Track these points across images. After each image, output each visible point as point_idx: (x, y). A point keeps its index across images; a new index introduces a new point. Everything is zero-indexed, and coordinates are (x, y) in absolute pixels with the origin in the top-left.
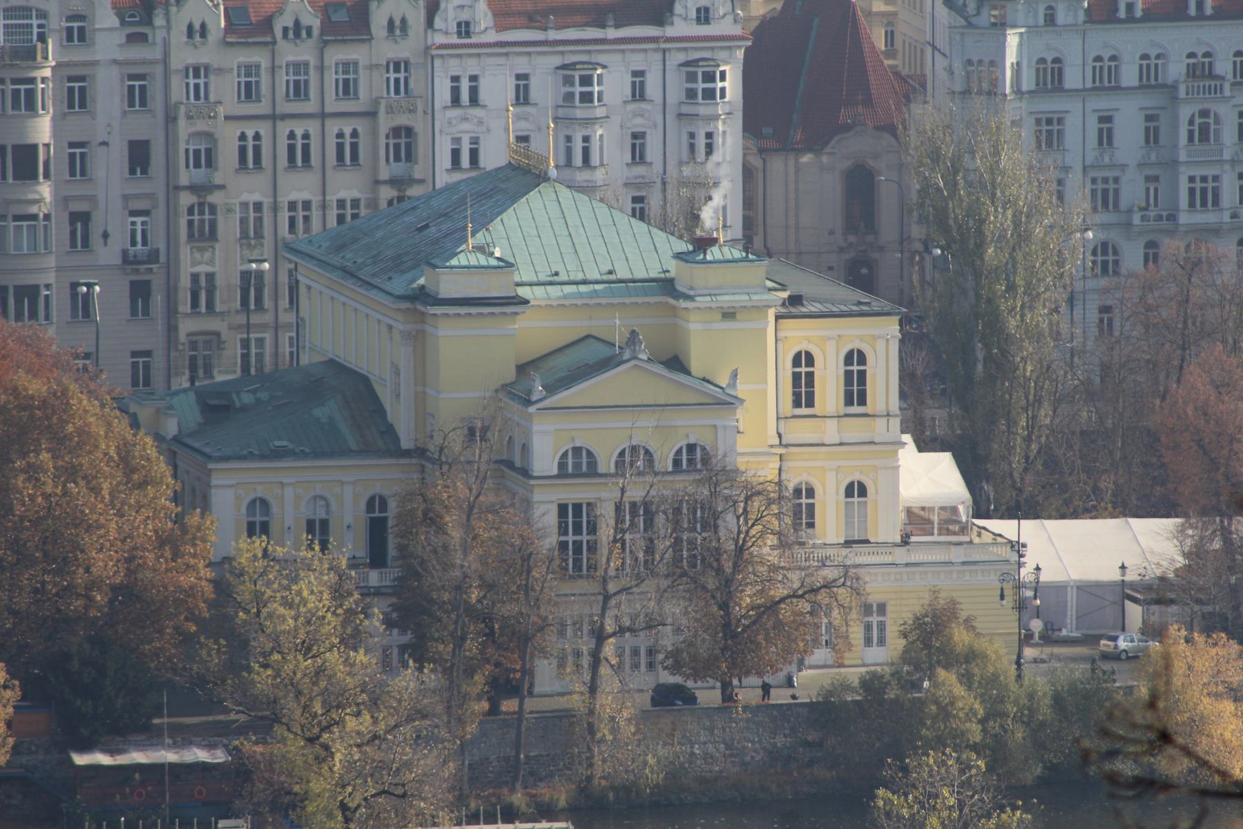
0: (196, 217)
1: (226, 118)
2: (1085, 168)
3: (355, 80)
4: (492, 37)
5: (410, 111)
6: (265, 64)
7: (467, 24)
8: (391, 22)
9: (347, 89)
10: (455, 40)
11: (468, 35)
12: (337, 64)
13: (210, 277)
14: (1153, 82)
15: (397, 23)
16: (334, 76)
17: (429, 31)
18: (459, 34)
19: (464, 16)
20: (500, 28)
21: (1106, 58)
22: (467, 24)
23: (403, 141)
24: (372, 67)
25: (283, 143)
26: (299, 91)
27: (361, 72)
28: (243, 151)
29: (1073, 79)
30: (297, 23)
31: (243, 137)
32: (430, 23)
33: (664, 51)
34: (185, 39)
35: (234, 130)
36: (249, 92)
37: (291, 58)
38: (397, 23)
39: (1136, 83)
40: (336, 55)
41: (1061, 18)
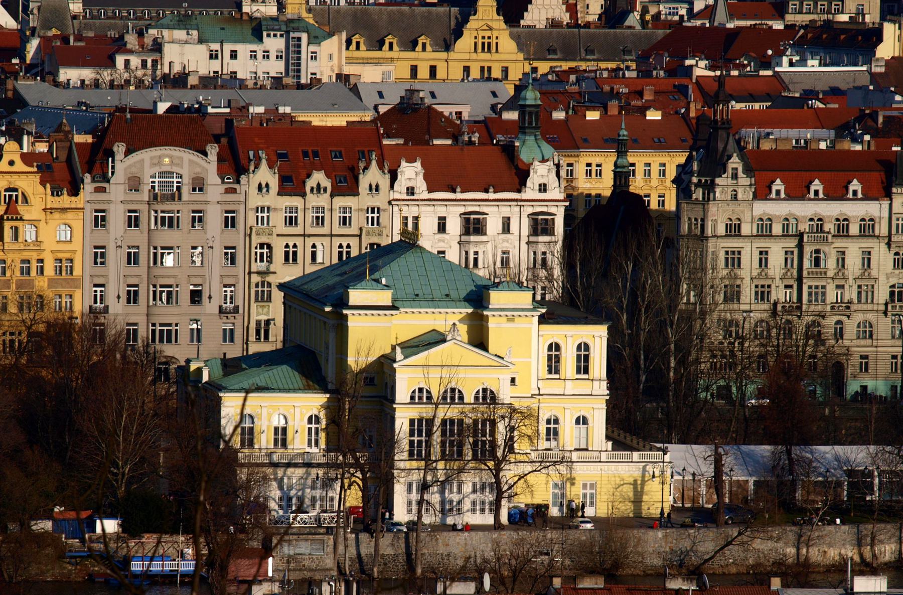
1: (278, 235)
3: (350, 217)
8: (260, 185)
10: (405, 197)
11: (413, 194)
18: (408, 193)
19: (410, 184)
20: (430, 190)
26: (320, 221)
28: (287, 253)
29: (746, 229)
30: (319, 185)
31: (287, 246)
34: (257, 191)
35: (283, 241)
36: (291, 221)
37: (314, 204)
40: (341, 202)
41: (740, 196)
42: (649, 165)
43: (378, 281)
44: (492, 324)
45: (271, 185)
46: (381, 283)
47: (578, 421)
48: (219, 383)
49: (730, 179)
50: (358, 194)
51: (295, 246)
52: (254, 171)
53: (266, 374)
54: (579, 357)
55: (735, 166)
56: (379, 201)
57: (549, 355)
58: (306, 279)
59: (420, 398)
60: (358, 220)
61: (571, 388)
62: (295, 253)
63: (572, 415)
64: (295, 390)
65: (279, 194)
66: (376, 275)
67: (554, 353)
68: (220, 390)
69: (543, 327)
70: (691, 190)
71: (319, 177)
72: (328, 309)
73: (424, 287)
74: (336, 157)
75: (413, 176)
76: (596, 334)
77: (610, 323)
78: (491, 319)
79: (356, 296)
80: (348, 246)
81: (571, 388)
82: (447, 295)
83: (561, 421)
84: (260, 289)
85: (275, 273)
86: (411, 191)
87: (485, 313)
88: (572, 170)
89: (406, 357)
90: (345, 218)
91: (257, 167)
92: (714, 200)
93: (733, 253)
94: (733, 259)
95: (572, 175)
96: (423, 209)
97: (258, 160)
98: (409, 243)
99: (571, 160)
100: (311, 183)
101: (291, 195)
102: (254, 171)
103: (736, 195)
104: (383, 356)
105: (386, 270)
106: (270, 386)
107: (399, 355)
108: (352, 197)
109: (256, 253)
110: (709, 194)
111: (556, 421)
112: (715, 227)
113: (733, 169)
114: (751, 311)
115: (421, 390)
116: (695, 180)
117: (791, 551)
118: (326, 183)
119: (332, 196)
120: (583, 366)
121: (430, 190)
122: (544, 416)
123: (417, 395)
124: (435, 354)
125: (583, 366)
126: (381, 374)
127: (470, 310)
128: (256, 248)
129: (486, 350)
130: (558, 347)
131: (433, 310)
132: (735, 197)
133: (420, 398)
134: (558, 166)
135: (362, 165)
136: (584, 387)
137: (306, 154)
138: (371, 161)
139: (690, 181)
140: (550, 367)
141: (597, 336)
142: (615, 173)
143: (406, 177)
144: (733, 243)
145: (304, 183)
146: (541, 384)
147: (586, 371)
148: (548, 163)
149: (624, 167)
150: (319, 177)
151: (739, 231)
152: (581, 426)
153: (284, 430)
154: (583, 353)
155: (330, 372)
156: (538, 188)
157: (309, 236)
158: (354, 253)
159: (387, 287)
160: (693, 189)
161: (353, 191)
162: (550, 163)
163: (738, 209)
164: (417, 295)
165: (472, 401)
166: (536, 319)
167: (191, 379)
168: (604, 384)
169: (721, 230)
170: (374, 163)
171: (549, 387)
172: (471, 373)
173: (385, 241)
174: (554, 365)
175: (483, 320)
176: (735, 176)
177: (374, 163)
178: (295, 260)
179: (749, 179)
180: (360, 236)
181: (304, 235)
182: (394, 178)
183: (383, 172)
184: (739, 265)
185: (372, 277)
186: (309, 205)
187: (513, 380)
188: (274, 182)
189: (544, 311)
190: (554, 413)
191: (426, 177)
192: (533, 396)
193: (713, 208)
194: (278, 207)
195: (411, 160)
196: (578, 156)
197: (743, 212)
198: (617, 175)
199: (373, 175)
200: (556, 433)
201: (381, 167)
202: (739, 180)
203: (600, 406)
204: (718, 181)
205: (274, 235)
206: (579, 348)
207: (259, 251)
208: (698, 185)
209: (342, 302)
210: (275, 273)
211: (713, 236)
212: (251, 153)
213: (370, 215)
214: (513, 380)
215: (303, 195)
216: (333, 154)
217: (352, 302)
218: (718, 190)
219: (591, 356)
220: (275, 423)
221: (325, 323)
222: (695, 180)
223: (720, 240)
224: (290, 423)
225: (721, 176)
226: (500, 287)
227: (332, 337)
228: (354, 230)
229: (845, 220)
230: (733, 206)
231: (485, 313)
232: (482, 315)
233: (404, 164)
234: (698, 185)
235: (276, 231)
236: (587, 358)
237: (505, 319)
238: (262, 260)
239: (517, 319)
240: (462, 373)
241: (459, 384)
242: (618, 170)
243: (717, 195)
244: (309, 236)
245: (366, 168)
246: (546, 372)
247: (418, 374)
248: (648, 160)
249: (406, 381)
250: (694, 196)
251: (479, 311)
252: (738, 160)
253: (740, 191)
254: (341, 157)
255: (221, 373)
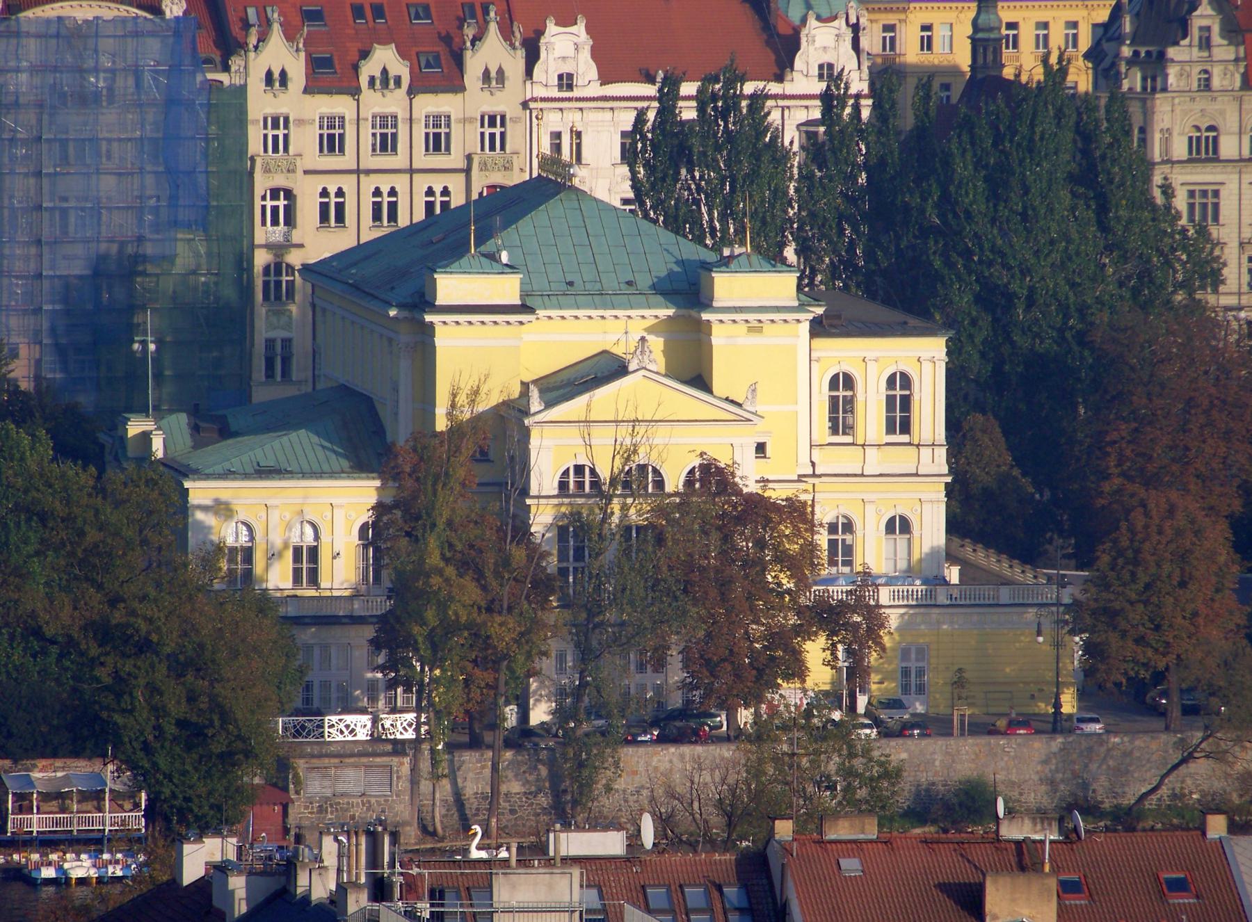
0: (272, 278)
1: (306, 172)
2: (1241, 244)
3: (448, 135)
4: (596, 90)
5: (506, 169)
6: (350, 115)
7: (570, 76)
8: (269, 74)
9: (437, 143)
10: (555, 93)
11: (570, 87)
12: (374, 117)
13: (287, 342)
14: (1204, 156)
15: (276, 75)
16: (371, 131)
17: (528, 83)
18: (560, 87)
19: (566, 68)
20: (605, 80)
21: (1203, 127)
22: (570, 76)
23: (281, 203)
24: (465, 121)
25: (368, 201)
26: (386, 144)
27: (453, 125)
28: (324, 208)
29: (1228, 147)
30: (385, 71)
31: (324, 193)
32: (529, 73)
33: (783, 108)
34: (480, 84)
35: (319, 183)
36: (332, 144)
37: (377, 110)
38: (276, 75)
39: (1185, 156)
40: (428, 104)
41: (1216, 82)
42: (1045, 25)
43: (493, 257)
44: (719, 337)
45: (508, 73)
46: (498, 261)
47: (890, 527)
48: (185, 462)
49: (1195, 50)
50: (462, 89)
51: (340, 193)
52: (256, 47)
53: (276, 444)
54: (890, 400)
55: (1205, 22)
56: (504, 102)
57: (888, 397)
58: (360, 254)
59: (580, 485)
60: (464, 139)
61: (875, 461)
62: (340, 208)
63: (878, 512)
64: (333, 474)
65: (307, 91)
66: (489, 246)
67: (841, 393)
68: (186, 476)
69: (820, 343)
70: (1118, 73)
71: (385, 57)
72: (392, 313)
73: (584, 268)
74: (418, 17)
75: (570, 51)
76: (925, 355)
77: (951, 333)
78: (716, 329)
79: (451, 286)
80: (445, 192)
81: (875, 461)
82: (629, 283)
83: (858, 526)
84: (272, 278)
85: (301, 246)
86: (566, 81)
87: (705, 316)
88: (893, 39)
89: (549, 405)
90: (437, 136)
91: (262, 39)
92: (1164, 90)
93: (1204, 193)
94: (1204, 206)
95: (893, 47)
96: (592, 116)
97: (266, 24)
98: (555, 182)
99: (891, 19)
100: (369, 68)
101: (329, 93)
102: (256, 47)
103: (1208, 80)
104: (504, 403)
105: (511, 234)
106: (284, 465)
107: (535, 404)
108: (325, 97)
109: (264, 207)
110: (1154, 79)
111: (849, 527)
112: (1167, 142)
113: (1201, 29)
114: (1240, 309)
115: (579, 469)
116: (1126, 51)
117: (36, 775)
118: (400, 68)
119: (411, 92)
120: (900, 417)
121: (605, 80)
122: (824, 514)
123: (572, 479)
124: (605, 399)
125: (900, 417)
126: (499, 438)
127: (671, 312)
128: (264, 198)
129: (708, 389)
130: (849, 381)
131: (601, 312)
132: (1206, 85)
133: (580, 485)
134: (856, 28)
135: (469, 32)
136: (903, 460)
137: (358, 11)
138: (487, 23)
139: (1117, 55)
140: (834, 421)
141: (925, 358)
142: (975, 41)
143: (557, 54)
144: (1204, 175)
145: (356, 68)
146: (817, 455)
147: (906, 428)
148: (836, 23)
149: (991, 29)
150: (385, 57)
151: (1216, 150)
152: (898, 536)
153: (314, 552)
154: (898, 392)
155: (401, 433)
156: (816, 72)
157: (368, 172)
158: (457, 200)
159: (511, 268)
160: (1123, 68)
161: (455, 85)
162: (840, 23)
163: (1212, 107)
164: (571, 284)
165: (556, 492)
166: (806, 326)
167: (130, 454)
168: (942, 453)
169: (1180, 149)
170: (493, 27)
171: (830, 461)
172: (677, 436)
173: (516, 178)
174: (841, 415)
175: (704, 330)
176: (1206, 44)
177: (493, 27)
178: (340, 218)
179: (1232, 48)
180: (467, 171)
181: (358, 172)
182: (532, 57)
183: (512, 46)
184: (1216, 218)
185: (482, 249)
186: (367, 113)
187: (761, 448)
188: (297, 69)
189: (820, 311)
190: (843, 510)
191: (595, 54)
192: (801, 478)
193: (1162, 104)
194: (306, 116)
195: (566, 21)
196: (904, 10)
197: (1222, 113)
198: (977, 44)
199: (491, 52)
200: (848, 550)
201: (507, 34)
202: (1215, 51)
203: (933, 496)
204: (1172, 52)
205: (299, 172)
206: (891, 382)
207: (269, 203)
208: (1134, 61)
209: (423, 301)
210: (301, 246)
211: (1163, 162)
212: (251, 12)
213: (488, 131)
214: (761, 448)
215: (355, 92)
216: (412, 11)
217: (442, 299)
218: (1172, 72)
219: (860, 398)
220: (295, 540)
221: (390, 340)
222: (1126, 51)
223: (1177, 168)
224: (325, 538)
225: (1176, 43)
226: (733, 266)
227: (405, 369)
228: (455, 159)
229: (1211, 128)
230: (1202, 103)
231: (705, 316)
232: (699, 322)
233: (552, 28)
234: (1134, 61)
235: (301, 165)
236: (906, 402)
237: (743, 328)
238: (275, 222)
239: (767, 327)
240: (660, 435)
241: (654, 455)
242: (980, 35)
243: (1172, 80)
244: (368, 172)
245: (476, 39)
246: (827, 431)
247: (572, 435)
248: (1043, 16)
249: (552, 452)
250: (1126, 85)
251: (693, 313)
252: (1210, 11)
253: (1217, 71)
254: (428, 16)
255: (189, 442)
